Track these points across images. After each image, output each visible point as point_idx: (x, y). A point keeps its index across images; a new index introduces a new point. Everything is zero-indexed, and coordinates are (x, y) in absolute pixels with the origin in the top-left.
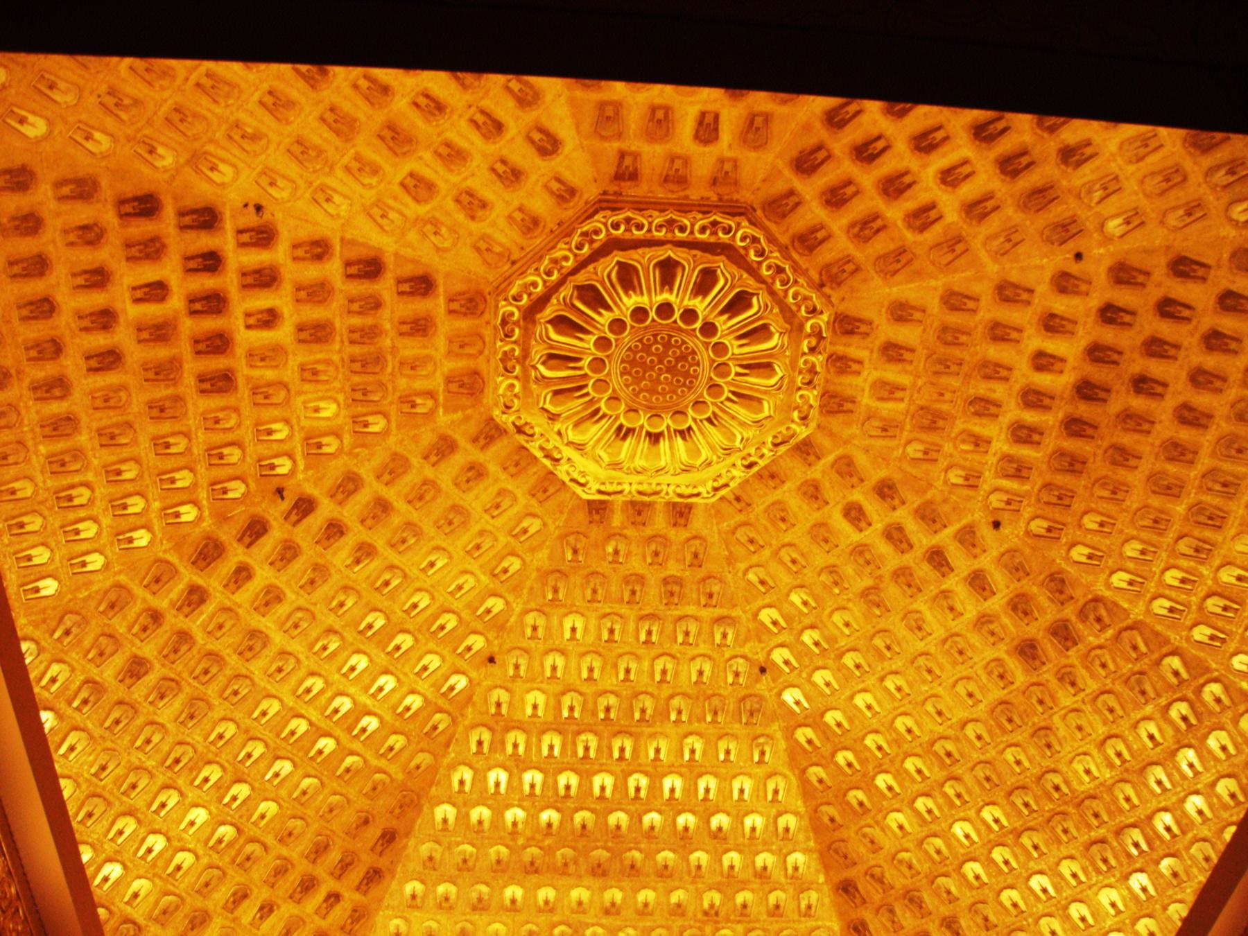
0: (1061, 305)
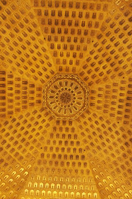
0: (123, 85)
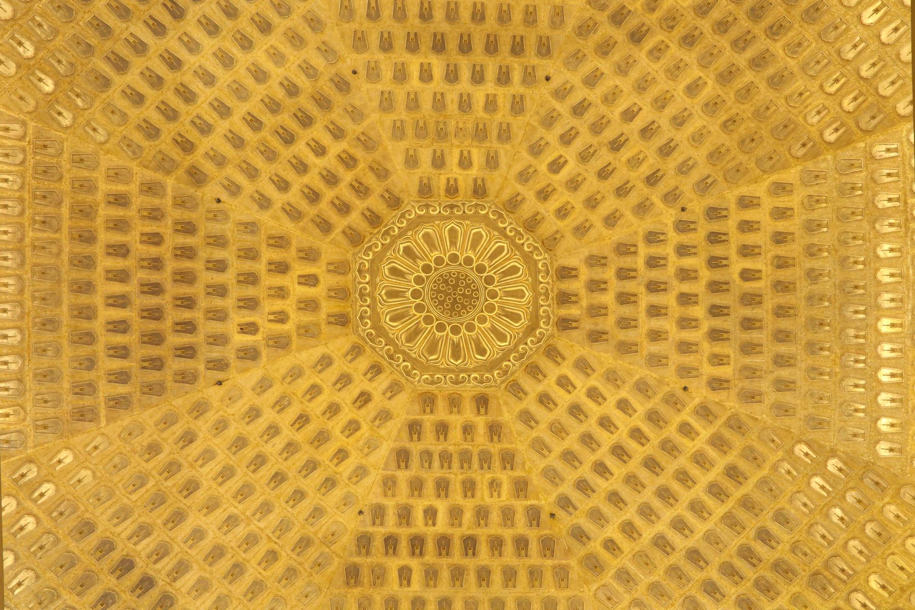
0: (387, 73)
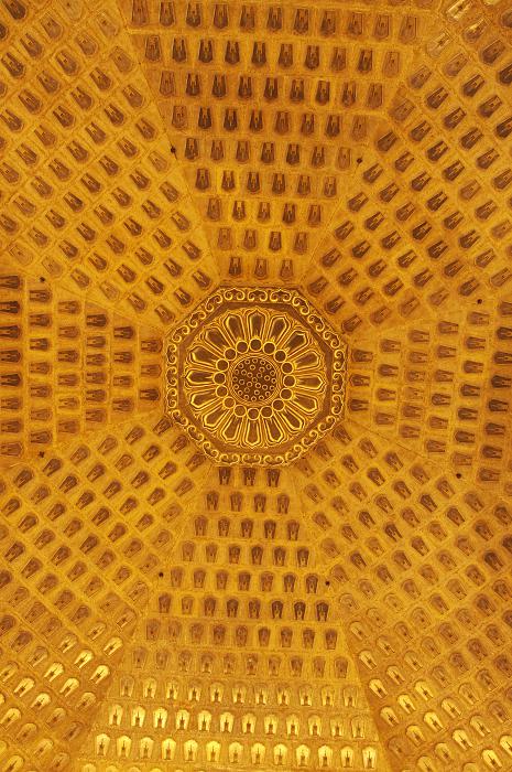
0: (475, 332)
